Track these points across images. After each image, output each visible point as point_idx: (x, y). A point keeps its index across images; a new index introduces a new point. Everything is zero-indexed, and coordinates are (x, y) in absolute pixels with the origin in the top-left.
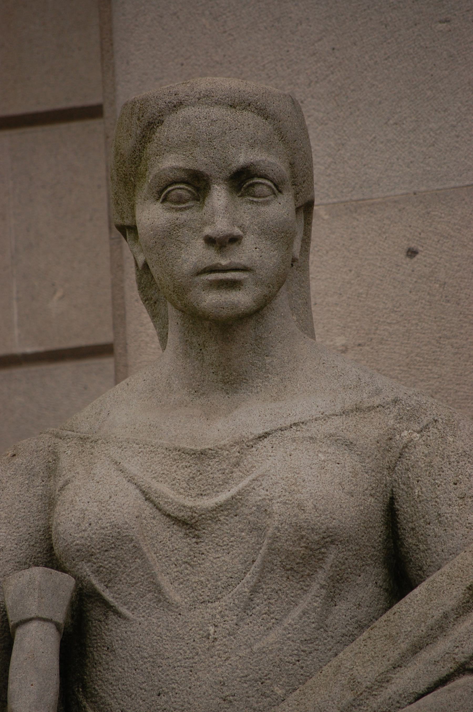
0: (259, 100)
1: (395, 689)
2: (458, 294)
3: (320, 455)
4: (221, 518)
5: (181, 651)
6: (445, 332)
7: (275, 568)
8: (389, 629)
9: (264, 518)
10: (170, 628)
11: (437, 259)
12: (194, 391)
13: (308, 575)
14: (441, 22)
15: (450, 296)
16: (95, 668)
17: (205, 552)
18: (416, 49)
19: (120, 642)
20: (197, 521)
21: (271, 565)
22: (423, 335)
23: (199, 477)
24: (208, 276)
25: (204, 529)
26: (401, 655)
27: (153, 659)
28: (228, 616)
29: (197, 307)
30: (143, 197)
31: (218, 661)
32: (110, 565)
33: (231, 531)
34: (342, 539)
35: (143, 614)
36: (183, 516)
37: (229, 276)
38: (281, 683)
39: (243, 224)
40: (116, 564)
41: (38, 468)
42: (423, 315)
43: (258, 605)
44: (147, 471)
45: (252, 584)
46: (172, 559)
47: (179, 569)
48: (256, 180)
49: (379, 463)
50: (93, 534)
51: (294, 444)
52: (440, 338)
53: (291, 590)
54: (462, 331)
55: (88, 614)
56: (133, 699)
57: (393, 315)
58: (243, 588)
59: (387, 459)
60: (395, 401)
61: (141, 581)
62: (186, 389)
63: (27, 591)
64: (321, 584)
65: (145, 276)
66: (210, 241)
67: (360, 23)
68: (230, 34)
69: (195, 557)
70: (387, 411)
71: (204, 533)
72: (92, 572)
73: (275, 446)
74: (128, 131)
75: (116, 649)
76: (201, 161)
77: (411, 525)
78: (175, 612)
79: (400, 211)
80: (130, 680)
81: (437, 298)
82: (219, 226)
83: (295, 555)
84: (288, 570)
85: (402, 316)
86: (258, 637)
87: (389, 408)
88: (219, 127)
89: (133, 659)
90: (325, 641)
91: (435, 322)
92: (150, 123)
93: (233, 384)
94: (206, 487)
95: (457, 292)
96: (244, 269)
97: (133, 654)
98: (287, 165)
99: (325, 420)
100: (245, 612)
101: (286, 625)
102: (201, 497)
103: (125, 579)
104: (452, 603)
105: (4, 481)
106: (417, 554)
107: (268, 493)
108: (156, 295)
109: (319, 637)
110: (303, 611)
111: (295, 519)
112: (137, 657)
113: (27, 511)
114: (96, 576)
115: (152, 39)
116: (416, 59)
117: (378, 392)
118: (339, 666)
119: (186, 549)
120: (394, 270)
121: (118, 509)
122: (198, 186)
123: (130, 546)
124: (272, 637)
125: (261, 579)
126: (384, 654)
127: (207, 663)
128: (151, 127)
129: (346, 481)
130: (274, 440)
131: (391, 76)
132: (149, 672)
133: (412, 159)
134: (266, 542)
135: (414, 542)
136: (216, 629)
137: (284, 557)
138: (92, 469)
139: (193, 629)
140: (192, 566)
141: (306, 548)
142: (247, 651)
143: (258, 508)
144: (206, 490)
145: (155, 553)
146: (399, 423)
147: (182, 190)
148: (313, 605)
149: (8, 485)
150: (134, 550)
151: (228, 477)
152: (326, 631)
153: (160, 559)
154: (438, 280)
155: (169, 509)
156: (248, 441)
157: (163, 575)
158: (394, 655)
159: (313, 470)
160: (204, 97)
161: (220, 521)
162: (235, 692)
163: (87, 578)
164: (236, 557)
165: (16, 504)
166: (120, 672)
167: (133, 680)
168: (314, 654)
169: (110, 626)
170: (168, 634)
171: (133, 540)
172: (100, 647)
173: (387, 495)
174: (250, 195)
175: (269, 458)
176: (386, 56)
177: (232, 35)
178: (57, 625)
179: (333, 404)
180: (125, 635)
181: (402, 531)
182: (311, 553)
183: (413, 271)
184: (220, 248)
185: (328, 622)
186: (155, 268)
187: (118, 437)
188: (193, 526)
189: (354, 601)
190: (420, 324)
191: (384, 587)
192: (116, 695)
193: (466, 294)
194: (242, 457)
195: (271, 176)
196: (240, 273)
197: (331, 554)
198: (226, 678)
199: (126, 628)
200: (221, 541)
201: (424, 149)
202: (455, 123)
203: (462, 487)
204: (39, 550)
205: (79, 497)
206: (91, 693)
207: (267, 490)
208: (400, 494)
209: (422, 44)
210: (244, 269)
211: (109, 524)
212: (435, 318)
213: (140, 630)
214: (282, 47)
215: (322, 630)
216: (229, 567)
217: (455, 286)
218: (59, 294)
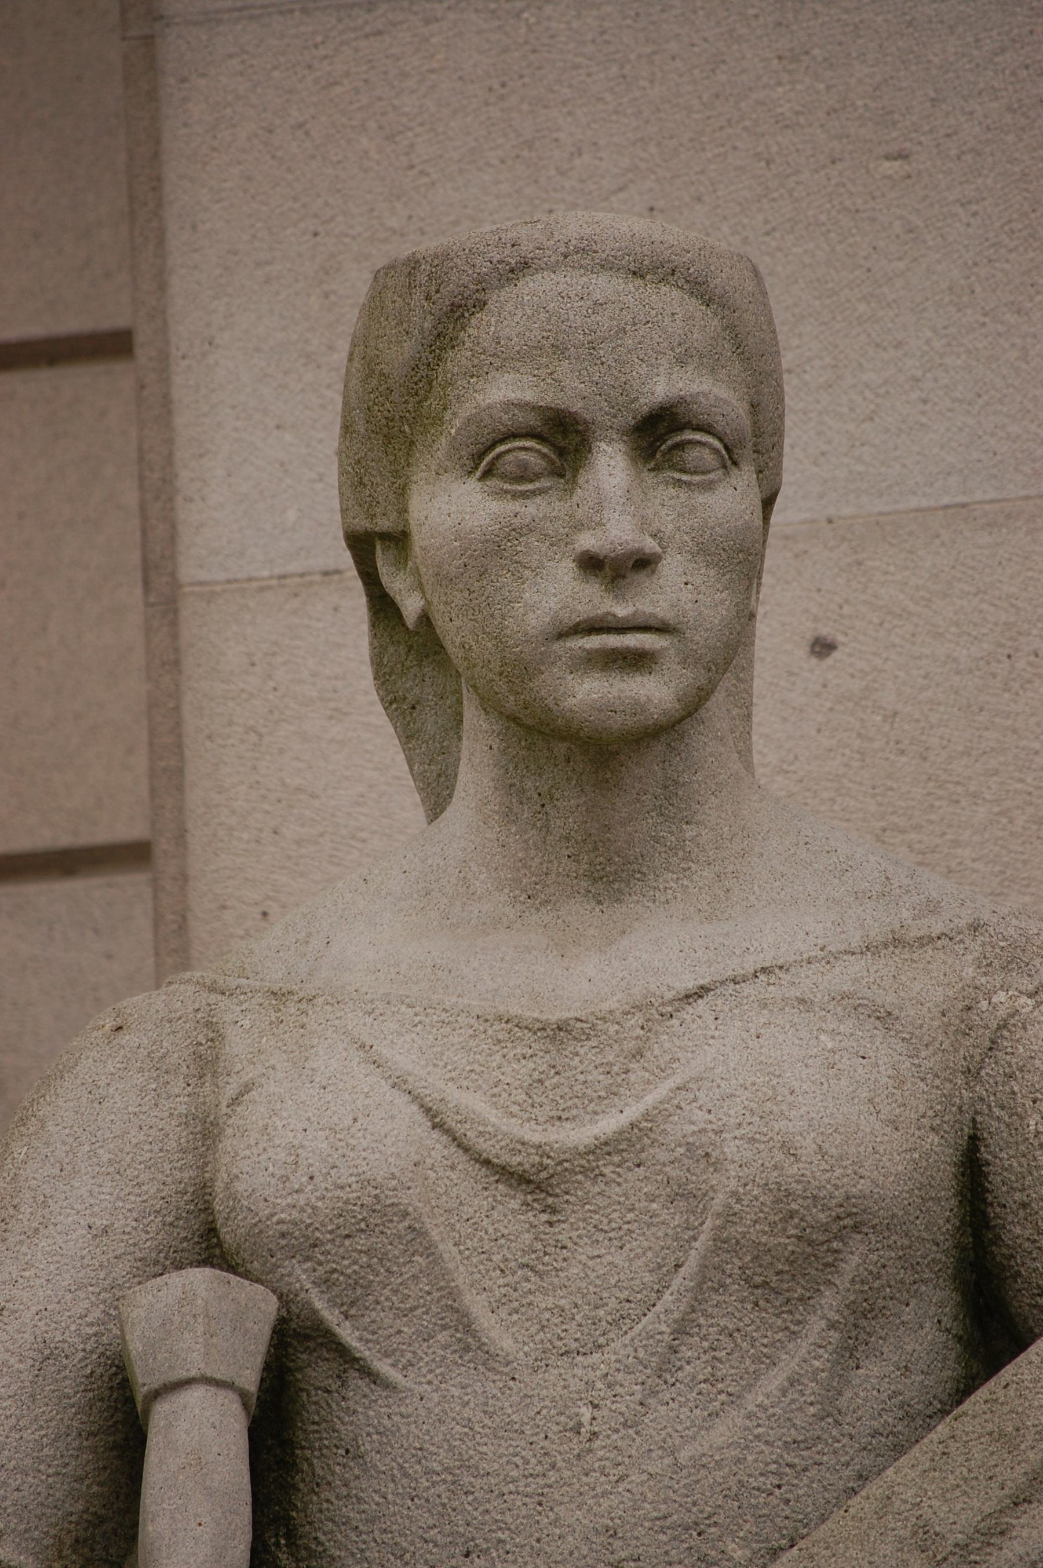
0: (692, 262)
1: (1021, 1551)
2: (924, 738)
3: (823, 1037)
4: (607, 1171)
5: (517, 1460)
6: (895, 819)
7: (728, 1281)
8: (997, 1420)
9: (704, 1171)
10: (491, 1409)
11: (878, 662)
12: (524, 896)
13: (801, 1299)
14: (888, 157)
15: (907, 742)
16: (317, 1494)
17: (570, 1245)
18: (834, 213)
19: (375, 1437)
20: (552, 1176)
21: (719, 1276)
22: (845, 824)
23: (555, 1080)
24: (585, 640)
25: (567, 1193)
26: (1031, 1476)
27: (454, 1475)
28: (621, 1385)
29: (555, 708)
30: (433, 467)
31: (602, 1484)
32: (356, 1267)
33: (627, 1198)
34: (877, 1221)
35: (429, 1377)
36: (520, 1164)
38: (741, 1534)
39: (660, 531)
40: (369, 1266)
41: (176, 1055)
42: (845, 781)
43: (688, 1363)
44: (435, 1065)
45: (676, 1315)
46: (494, 1258)
47: (510, 1279)
48: (689, 435)
49: (948, 1060)
50: (319, 1199)
51: (765, 1012)
52: (884, 830)
53: (762, 1331)
54: (933, 817)
55: (299, 1376)
56: (407, 1564)
57: (779, 779)
58: (657, 1323)
59: (962, 1052)
60: (975, 928)
61: (424, 1305)
62: (506, 891)
63: (177, 1319)
64: (829, 1320)
65: (391, 649)
66: (591, 564)
67: (709, 155)
68: (421, 172)
69: (546, 1254)
70: (959, 948)
71: (567, 1201)
72: (314, 1283)
73: (722, 1016)
74: (400, 323)
75: (367, 1452)
76: (571, 390)
77: (1018, 1196)
78: (502, 1373)
79: (797, 556)
80: (400, 1521)
81: (877, 745)
82: (614, 532)
83: (773, 1253)
84: (756, 1287)
85: (801, 781)
86: (690, 1433)
87: (961, 941)
88: (611, 319)
89: (406, 1475)
90: (836, 1445)
91: (874, 796)
92: (454, 307)
93: (613, 882)
94: (570, 1103)
95: (922, 734)
96: (662, 629)
97: (407, 1465)
98: (747, 407)
99: (828, 962)
100: (659, 1377)
101: (751, 1408)
102: (558, 1123)
103: (387, 1299)
105: (102, 1083)
106: (1034, 1259)
107: (711, 1117)
108: (417, 690)
109: (825, 1436)
110: (788, 1378)
111: (775, 1174)
112: (416, 1472)
113: (156, 1148)
114: (322, 1292)
115: (249, 179)
116: (833, 235)
117: (933, 907)
118: (889, 1498)
119: (527, 1236)
120: (782, 683)
121: (374, 1145)
122: (562, 444)
123: (400, 1226)
124: (721, 1433)
125: (696, 1304)
126: (990, 1474)
127: (577, 1486)
128: (457, 314)
129: (883, 1096)
130: (719, 1002)
131: (779, 268)
132: (444, 1505)
133: (825, 448)
134: (708, 1224)
135: (1027, 1233)
136: (596, 1413)
137: (749, 1258)
138: (307, 1059)
139: (544, 1412)
140: (540, 1274)
141: (800, 1238)
142: (666, 1461)
143: (688, 1150)
144: (569, 1108)
145: (455, 1245)
146: (985, 974)
147: (529, 454)
148: (811, 1366)
149: (111, 1091)
150: (410, 1237)
151: (619, 1080)
152: (838, 1423)
153: (467, 1258)
154: (880, 707)
155: (487, 1147)
156: (663, 1004)
157: (474, 1292)
159: (811, 1071)
160: (577, 253)
161: (603, 1175)
162: (640, 1551)
163: (303, 1295)
164: (637, 1257)
165: (133, 1132)
166: (377, 1504)
167: (407, 1522)
168: (813, 1473)
169: (351, 1403)
170: (487, 1421)
171: (408, 1214)
172: (327, 1447)
173: (962, 1130)
174: (673, 467)
175: (711, 1042)
176: (768, 227)
177: (428, 175)
178: (243, 1395)
179: (839, 930)
180: (386, 1421)
181: (998, 1210)
182: (809, 1250)
183: (825, 686)
184: (613, 580)
185: (842, 1402)
186: (457, 623)
187: (363, 990)
188: (543, 1185)
189: (896, 1359)
190: (839, 799)
191: (954, 1332)
192: (368, 1554)
193: (941, 738)
194: (648, 1039)
195: (720, 428)
196: (654, 636)
197: (852, 1253)
198: (617, 1521)
199: (388, 1406)
200: (606, 1221)
202: (919, 373)
204: (183, 1234)
205: (281, 1119)
206: (307, 1548)
207: (710, 1111)
208: (993, 1130)
209: (848, 203)
210: (662, 629)
211: (354, 1179)
212: (874, 788)
213: (422, 1412)
214: (537, 202)
215: (830, 1420)
216: (622, 1277)
217: (918, 721)
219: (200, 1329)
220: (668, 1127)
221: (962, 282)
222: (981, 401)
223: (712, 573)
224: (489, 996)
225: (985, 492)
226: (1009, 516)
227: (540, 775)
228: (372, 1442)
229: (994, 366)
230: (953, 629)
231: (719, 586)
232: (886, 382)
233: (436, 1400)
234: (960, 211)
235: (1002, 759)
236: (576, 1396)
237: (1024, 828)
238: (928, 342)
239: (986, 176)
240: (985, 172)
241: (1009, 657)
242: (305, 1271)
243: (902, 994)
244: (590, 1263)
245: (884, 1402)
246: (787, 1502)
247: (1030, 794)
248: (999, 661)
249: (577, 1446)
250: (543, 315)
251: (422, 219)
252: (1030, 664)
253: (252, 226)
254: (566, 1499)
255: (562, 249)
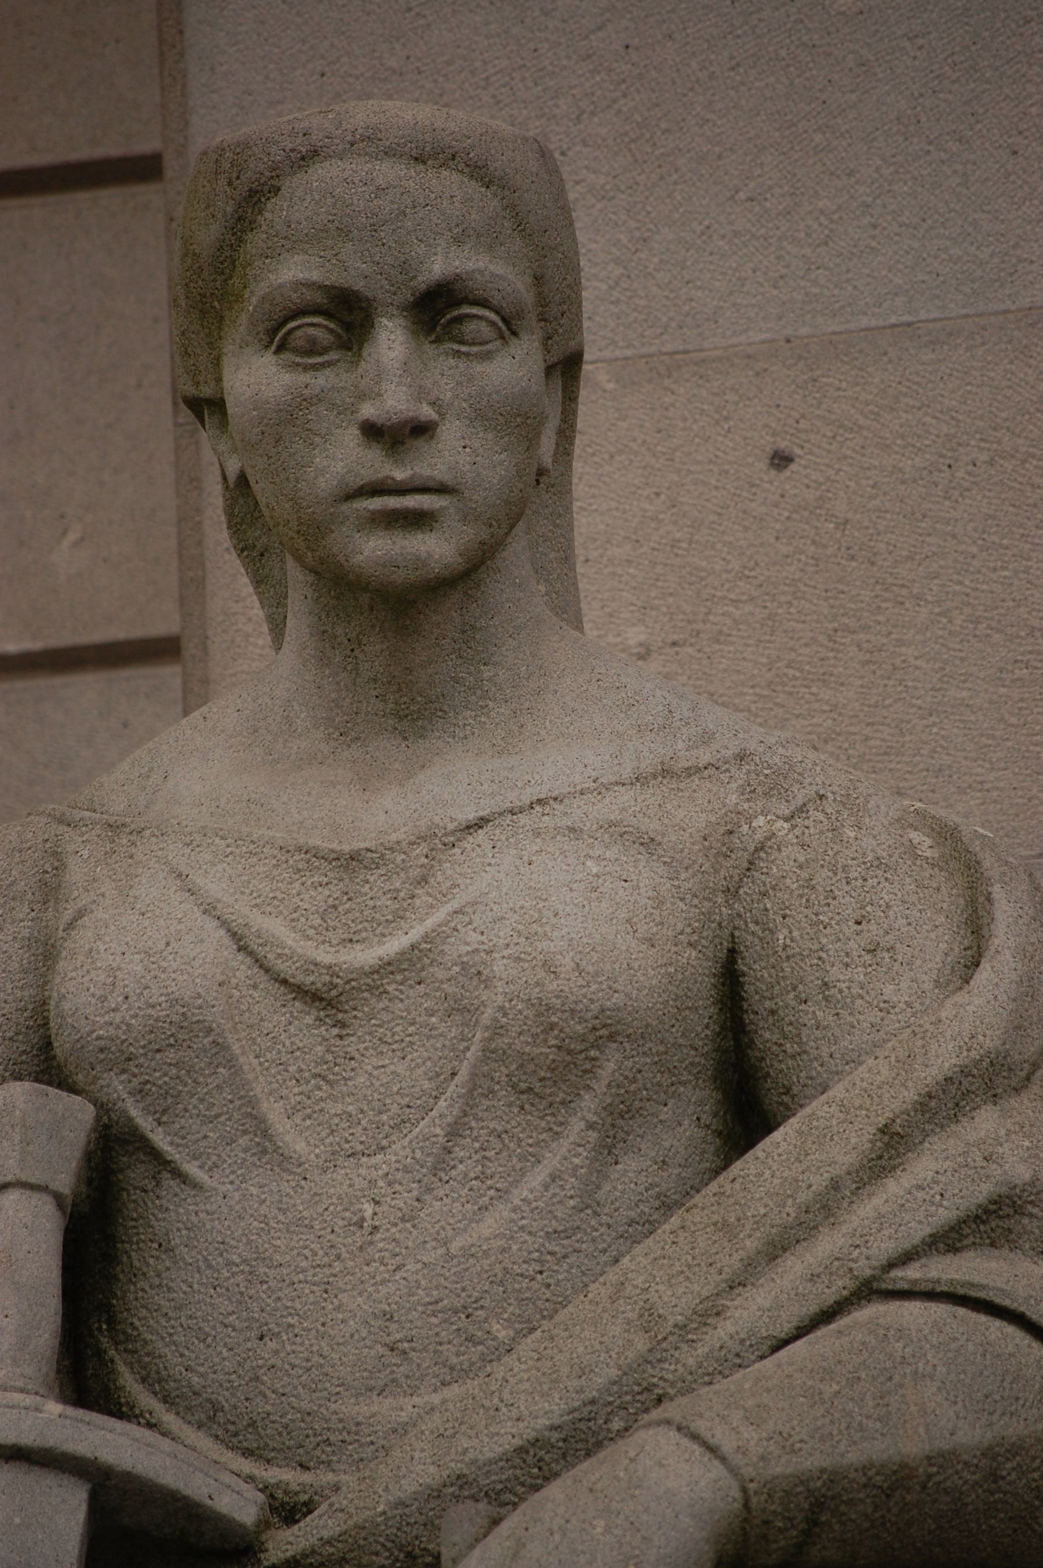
0: (472, 147)
2: (872, 544)
4: (390, 988)
5: (306, 1252)
7: (497, 1087)
8: (722, 1211)
9: (476, 988)
16: (134, 1284)
17: (357, 1056)
18: (793, 48)
19: (184, 1232)
31: (381, 1273)
32: (166, 1079)
33: (409, 1013)
34: (631, 1031)
35: (232, 1177)
36: (313, 983)
37: (411, 502)
38: (506, 1316)
42: (801, 585)
43: (461, 1162)
44: (242, 893)
45: (449, 1119)
46: (291, 1069)
48: (466, 310)
49: (708, 881)
54: (880, 618)
55: (121, 1177)
56: (209, 1346)
57: (741, 584)
58: (432, 1127)
59: (722, 873)
60: (742, 757)
62: (322, 729)
66: (372, 431)
69: (336, 1064)
71: (355, 1017)
72: (130, 1093)
74: (208, 207)
76: (354, 269)
77: (768, 1004)
79: (758, 374)
82: (390, 402)
84: (522, 1093)
87: (728, 770)
88: (392, 202)
89: (210, 1266)
91: (826, 599)
92: (252, 193)
94: (360, 927)
96: (442, 489)
98: (529, 280)
100: (435, 1175)
101: (517, 1202)
103: (195, 1107)
104: (848, 1159)
106: (780, 1061)
107: (483, 938)
108: (264, 539)
109: (584, 1226)
110: (550, 1175)
111: (537, 990)
115: (262, 22)
116: (792, 69)
117: (707, 738)
119: (319, 1048)
120: (745, 494)
123: (206, 1041)
124: (489, 1225)
129: (642, 916)
130: (497, 832)
132: (242, 1293)
133: (784, 271)
134: (478, 1036)
135: (775, 1037)
136: (377, 1209)
138: (131, 887)
139: (332, 1208)
141: (559, 1048)
143: (463, 969)
145: (256, 1057)
146: (748, 800)
147: (316, 329)
150: (214, 1051)
151: (405, 905)
154: (832, 516)
155: (283, 967)
156: (446, 835)
157: (272, 1100)
158: (732, 1262)
159: (574, 894)
163: (120, 1104)
164: (418, 1066)
166: (185, 1293)
168: (572, 1259)
169: (164, 1202)
170: (281, 1217)
175: (488, 869)
176: (733, 63)
177: (424, 17)
178: (58, 1197)
179: (616, 762)
180: (193, 1218)
181: (752, 1016)
182: (568, 1058)
185: (600, 1196)
189: (653, 1154)
190: (795, 603)
191: (713, 1127)
192: (175, 1338)
193: (888, 544)
194: (432, 866)
195: (495, 302)
197: (608, 1060)
199: (196, 1204)
200: (389, 1034)
201: (807, 251)
203: (872, 931)
204: (22, 1048)
206: (124, 1333)
207: (482, 933)
209: (805, 39)
210: (442, 489)
211: (163, 998)
212: (826, 591)
214: (523, 41)
215: (589, 1211)
216: (404, 1084)
217: (867, 528)
218: (72, 536)
219: (17, 1138)
220: (446, 948)
221: (909, 112)
222: (925, 226)
223: (490, 436)
224: (295, 828)
225: (928, 311)
226: (950, 334)
227: (349, 623)
228: (181, 1236)
229: (937, 192)
230: (899, 442)
231: (497, 448)
232: (839, 208)
233: (237, 1198)
234: (907, 44)
235: (942, 563)
236: (359, 1193)
237: (961, 626)
238: (877, 170)
239: (932, 12)
240: (930, 7)
241: (950, 466)
242: (122, 1082)
243: (666, 821)
244: (375, 1073)
245: (641, 1194)
246: (548, 1286)
247: (967, 595)
248: (940, 471)
249: (358, 1238)
250: (329, 201)
251: (419, 59)
252: (969, 474)
253: (265, 67)
254: (349, 1287)
255: (349, 138)
